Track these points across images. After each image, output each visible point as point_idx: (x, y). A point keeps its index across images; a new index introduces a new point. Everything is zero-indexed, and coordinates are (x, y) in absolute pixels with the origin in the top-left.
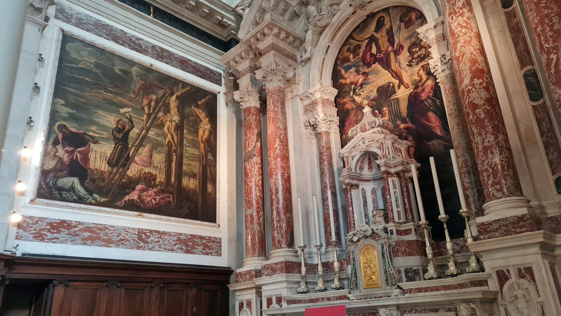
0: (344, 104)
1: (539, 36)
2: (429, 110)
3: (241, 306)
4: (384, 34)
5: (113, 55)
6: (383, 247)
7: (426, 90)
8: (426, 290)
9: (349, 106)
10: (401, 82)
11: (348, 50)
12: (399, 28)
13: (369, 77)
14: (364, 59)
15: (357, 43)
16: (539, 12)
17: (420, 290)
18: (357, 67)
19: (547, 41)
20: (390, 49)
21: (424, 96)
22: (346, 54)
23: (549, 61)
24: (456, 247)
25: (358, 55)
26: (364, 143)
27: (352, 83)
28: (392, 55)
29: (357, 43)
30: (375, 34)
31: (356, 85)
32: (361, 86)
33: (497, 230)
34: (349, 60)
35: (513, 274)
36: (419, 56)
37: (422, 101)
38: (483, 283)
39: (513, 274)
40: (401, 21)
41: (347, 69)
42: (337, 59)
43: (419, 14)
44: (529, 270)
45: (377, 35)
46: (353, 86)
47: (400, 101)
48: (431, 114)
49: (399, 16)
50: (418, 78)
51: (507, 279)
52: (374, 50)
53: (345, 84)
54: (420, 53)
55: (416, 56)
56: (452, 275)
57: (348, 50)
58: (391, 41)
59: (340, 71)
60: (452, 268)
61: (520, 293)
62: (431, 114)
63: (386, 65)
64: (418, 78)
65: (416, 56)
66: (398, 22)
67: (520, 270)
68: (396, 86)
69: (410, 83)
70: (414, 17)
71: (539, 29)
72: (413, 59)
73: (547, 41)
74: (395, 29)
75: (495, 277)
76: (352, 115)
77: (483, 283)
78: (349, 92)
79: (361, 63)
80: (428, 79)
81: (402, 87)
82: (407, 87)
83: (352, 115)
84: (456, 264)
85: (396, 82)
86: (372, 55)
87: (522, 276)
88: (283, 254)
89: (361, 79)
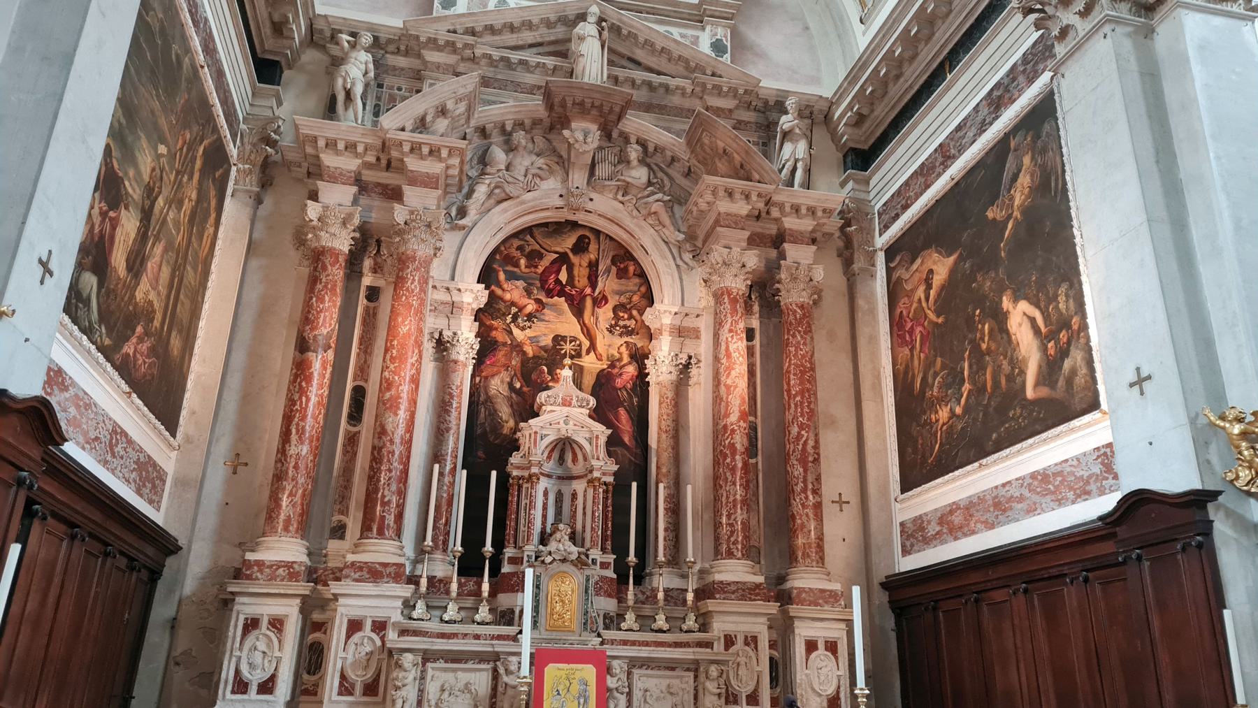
0: (491, 328)
1: (796, 405)
2: (621, 404)
3: (252, 624)
4: (585, 264)
5: (214, 41)
6: (588, 580)
7: (624, 377)
8: (633, 643)
9: (500, 336)
10: (593, 347)
11: (520, 248)
12: (608, 271)
13: (545, 311)
14: (543, 279)
15: (538, 247)
16: (801, 383)
17: (625, 643)
18: (530, 284)
19: (802, 415)
20: (588, 291)
21: (619, 383)
22: (517, 254)
23: (799, 436)
24: (640, 596)
25: (536, 267)
26: (566, 423)
27: (513, 304)
28: (589, 302)
29: (538, 247)
30: (571, 255)
31: (521, 310)
32: (530, 317)
33: (733, 592)
34: (517, 265)
35: (740, 640)
36: (625, 327)
37: (616, 389)
38: (709, 645)
39: (740, 640)
40: (613, 262)
41: (511, 277)
42: (496, 250)
43: (638, 272)
44: (755, 639)
45: (574, 259)
46: (514, 310)
47: (585, 372)
48: (622, 411)
49: (611, 254)
50: (617, 355)
51: (733, 644)
52: (563, 276)
53: (501, 299)
54: (627, 323)
55: (621, 323)
56: (660, 631)
57: (520, 248)
58: (593, 284)
59: (497, 272)
60: (661, 622)
61: (742, 660)
62: (622, 411)
63: (578, 312)
64: (617, 355)
65: (621, 323)
66: (609, 262)
67: (746, 637)
68: (584, 349)
69: (605, 357)
70: (631, 269)
71: (798, 398)
72: (616, 325)
73: (802, 415)
74: (602, 267)
75: (722, 640)
76: (502, 353)
77: (709, 645)
78: (505, 315)
79: (538, 283)
80: (630, 363)
81: (592, 354)
82: (599, 358)
83: (502, 353)
84: (638, 617)
85: (586, 343)
86: (558, 281)
87: (747, 644)
88: (393, 550)
89: (531, 307)
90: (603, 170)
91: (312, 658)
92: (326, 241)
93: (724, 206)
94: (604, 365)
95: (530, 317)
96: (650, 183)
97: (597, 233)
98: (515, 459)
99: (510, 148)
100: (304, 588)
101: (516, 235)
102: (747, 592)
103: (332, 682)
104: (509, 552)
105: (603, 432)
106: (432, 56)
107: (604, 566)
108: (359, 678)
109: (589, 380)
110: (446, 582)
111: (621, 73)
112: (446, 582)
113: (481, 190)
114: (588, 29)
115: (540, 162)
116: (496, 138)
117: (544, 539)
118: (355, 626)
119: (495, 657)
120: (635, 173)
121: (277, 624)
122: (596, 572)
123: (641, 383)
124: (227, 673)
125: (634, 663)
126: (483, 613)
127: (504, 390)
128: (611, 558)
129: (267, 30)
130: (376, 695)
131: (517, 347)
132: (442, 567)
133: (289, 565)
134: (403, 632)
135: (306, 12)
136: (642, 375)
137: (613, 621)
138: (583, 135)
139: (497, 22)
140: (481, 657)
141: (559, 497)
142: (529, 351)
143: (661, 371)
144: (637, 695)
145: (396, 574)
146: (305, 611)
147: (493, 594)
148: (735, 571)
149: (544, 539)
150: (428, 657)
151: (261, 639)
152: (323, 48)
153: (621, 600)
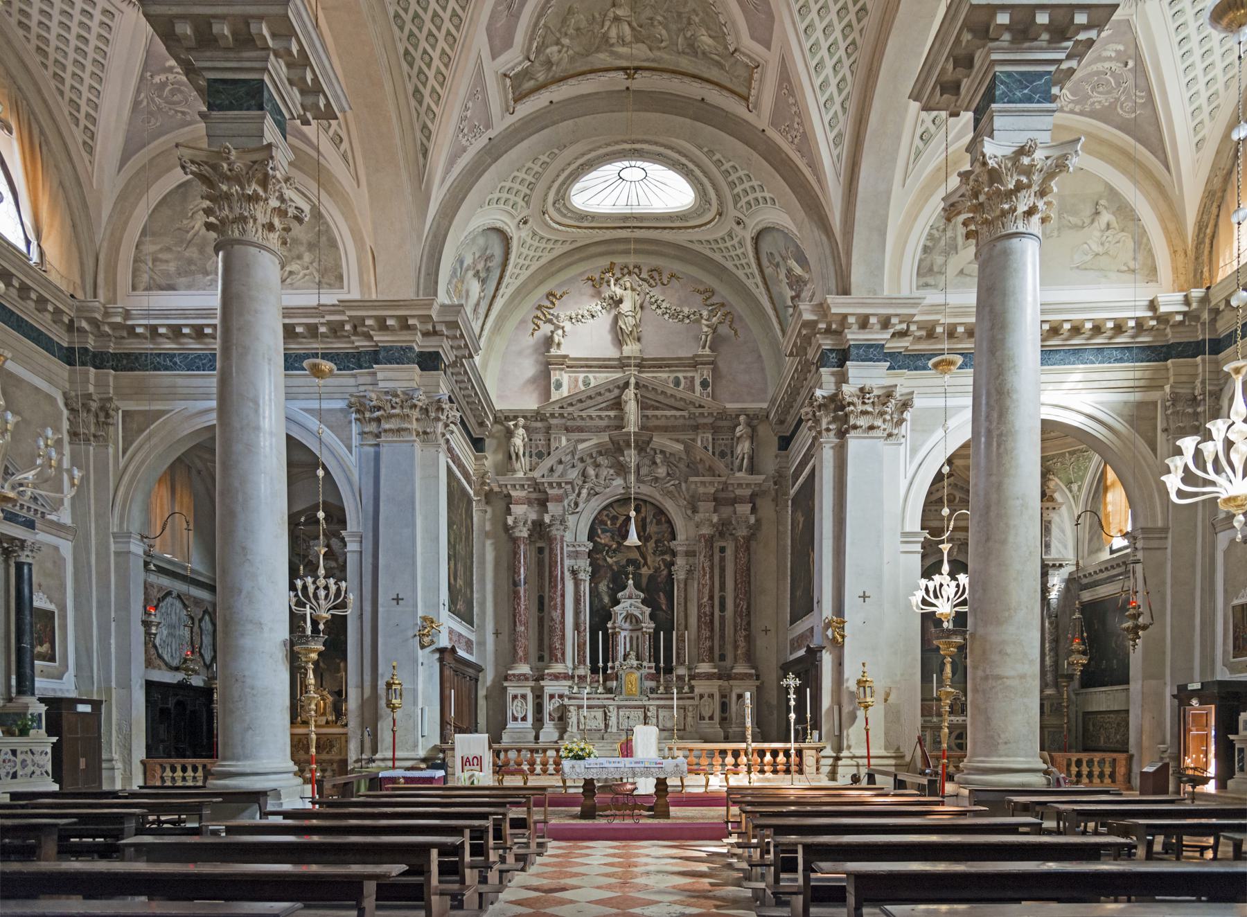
9: (601, 562)
10: (646, 563)
41: (604, 531)
90: (644, 471)
91: (539, 708)
92: (518, 534)
93: (701, 490)
94: (651, 572)
95: (614, 551)
96: (668, 474)
97: (645, 501)
98: (609, 625)
99: (597, 466)
100: (532, 684)
101: (605, 508)
102: (709, 677)
103: (546, 717)
104: (610, 664)
105: (648, 610)
106: (553, 421)
107: (650, 668)
108: (556, 716)
109: (644, 581)
110: (585, 677)
111: (649, 413)
112: (585, 677)
113: (585, 491)
114: (630, 393)
115: (612, 471)
116: (589, 461)
117: (625, 657)
118: (552, 697)
119: (604, 706)
120: (660, 470)
121: (524, 697)
122: (645, 671)
123: (670, 578)
124: (509, 715)
125: (658, 707)
126: (601, 690)
127: (605, 589)
128: (653, 665)
129: (476, 426)
130: (844, 887)
131: (610, 566)
132: (584, 670)
133: (524, 675)
134: (570, 698)
135: (491, 411)
136: (670, 574)
137: (653, 691)
138: (631, 457)
139: (583, 397)
140: (599, 707)
141: (631, 638)
142: (615, 568)
143: (680, 574)
144: (661, 718)
145: (566, 677)
146: (533, 689)
147: (605, 681)
148: (705, 668)
149: (625, 657)
150: (619, 707)
151: (518, 702)
152: (502, 424)
153: (658, 681)
